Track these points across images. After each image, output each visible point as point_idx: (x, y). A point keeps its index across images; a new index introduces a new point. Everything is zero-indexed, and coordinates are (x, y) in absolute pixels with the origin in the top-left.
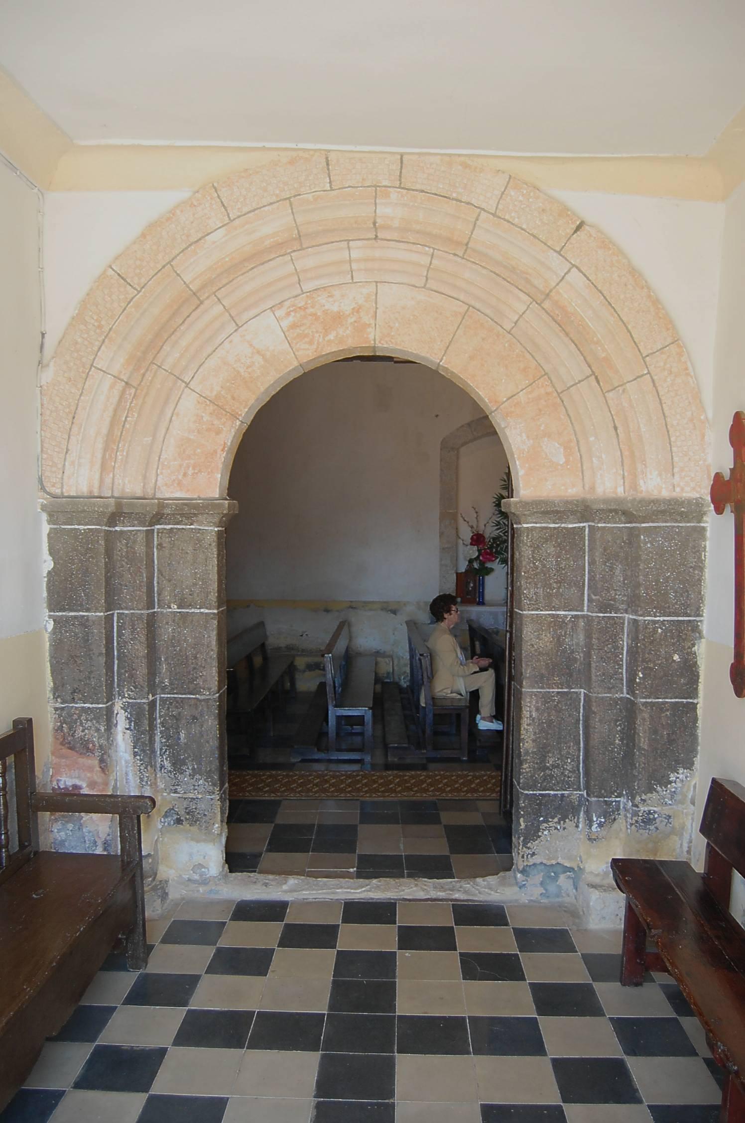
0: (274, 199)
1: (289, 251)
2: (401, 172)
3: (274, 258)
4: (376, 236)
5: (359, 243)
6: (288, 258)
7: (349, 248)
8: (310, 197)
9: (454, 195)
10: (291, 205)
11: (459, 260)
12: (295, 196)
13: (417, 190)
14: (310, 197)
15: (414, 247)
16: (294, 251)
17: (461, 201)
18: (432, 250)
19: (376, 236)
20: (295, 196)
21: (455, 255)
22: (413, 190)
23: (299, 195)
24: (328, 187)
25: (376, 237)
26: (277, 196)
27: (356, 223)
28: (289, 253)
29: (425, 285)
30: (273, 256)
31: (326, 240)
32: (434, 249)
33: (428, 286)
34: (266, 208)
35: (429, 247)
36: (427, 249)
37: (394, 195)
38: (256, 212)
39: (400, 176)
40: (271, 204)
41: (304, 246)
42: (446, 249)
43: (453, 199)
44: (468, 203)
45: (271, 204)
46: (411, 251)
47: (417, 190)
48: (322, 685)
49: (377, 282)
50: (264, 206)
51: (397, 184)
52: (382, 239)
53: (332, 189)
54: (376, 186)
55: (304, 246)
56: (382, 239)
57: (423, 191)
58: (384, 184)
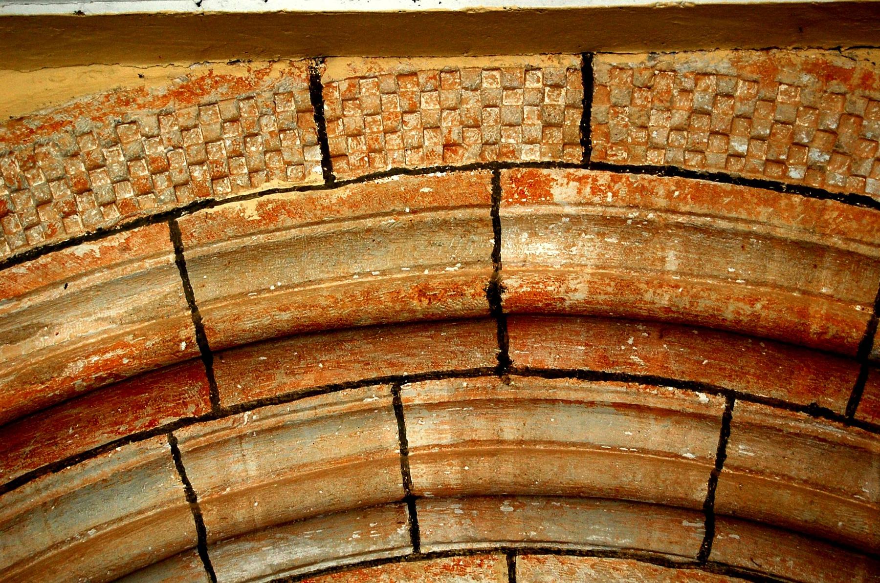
0: (114, 216)
1: (166, 421)
2: (586, 116)
3: (105, 449)
4: (504, 358)
5: (439, 390)
6: (160, 447)
7: (399, 410)
8: (250, 209)
9: (796, 174)
10: (176, 236)
11: (834, 431)
12: (193, 207)
13: (650, 170)
14: (250, 209)
15: (653, 397)
16: (186, 422)
17: (822, 194)
18: (721, 401)
19: (504, 358)
20: (193, 207)
21: (815, 411)
22: (636, 170)
23: (211, 203)
24: (316, 175)
25: (504, 368)
26: (125, 205)
27: (422, 293)
28: (168, 429)
29: (704, 553)
30: (102, 438)
31: (308, 381)
32: (731, 396)
33: (715, 555)
34: (81, 250)
35: (712, 390)
36: (703, 397)
37: (564, 190)
38: (42, 260)
39: (585, 129)
40: (102, 234)
41: (226, 403)
42: (776, 393)
43: (793, 189)
44: (852, 199)
45: (102, 234)
46: (640, 409)
47: (650, 170)
48: (854, 69)
49: (511, 553)
50: (75, 241)
51: (576, 154)
52: (527, 372)
53: (331, 183)
54: (496, 167)
55: (226, 403)
56: (527, 372)
57: (670, 171)
58: (525, 158)
